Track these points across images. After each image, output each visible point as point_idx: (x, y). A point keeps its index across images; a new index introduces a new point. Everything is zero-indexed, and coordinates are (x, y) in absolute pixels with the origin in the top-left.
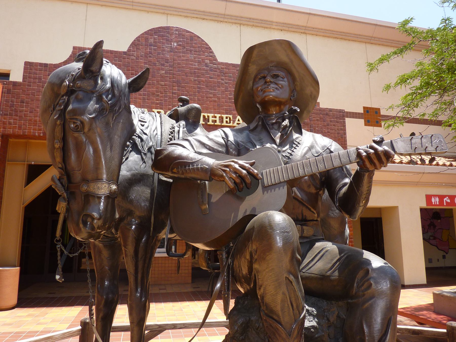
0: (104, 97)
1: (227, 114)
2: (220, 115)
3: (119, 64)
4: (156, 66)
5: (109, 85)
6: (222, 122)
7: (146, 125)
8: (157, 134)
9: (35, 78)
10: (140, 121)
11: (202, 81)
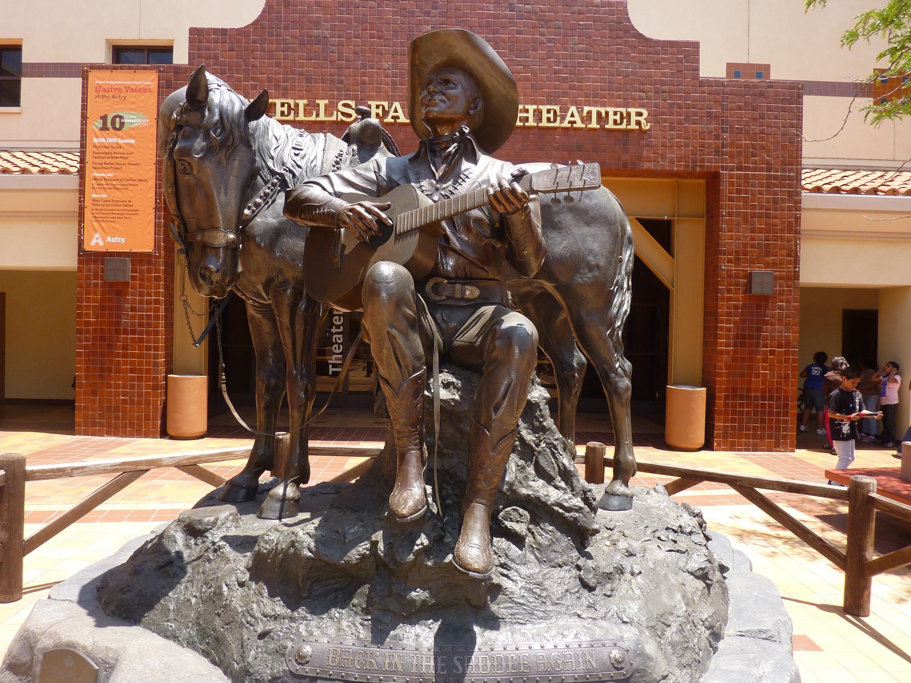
0: (211, 132)
1: (551, 104)
2: (535, 107)
3: (348, 17)
4: (414, 17)
5: (217, 117)
6: (540, 120)
7: (302, 153)
8: (315, 166)
9: (208, 58)
10: (294, 148)
11: (503, 41)
